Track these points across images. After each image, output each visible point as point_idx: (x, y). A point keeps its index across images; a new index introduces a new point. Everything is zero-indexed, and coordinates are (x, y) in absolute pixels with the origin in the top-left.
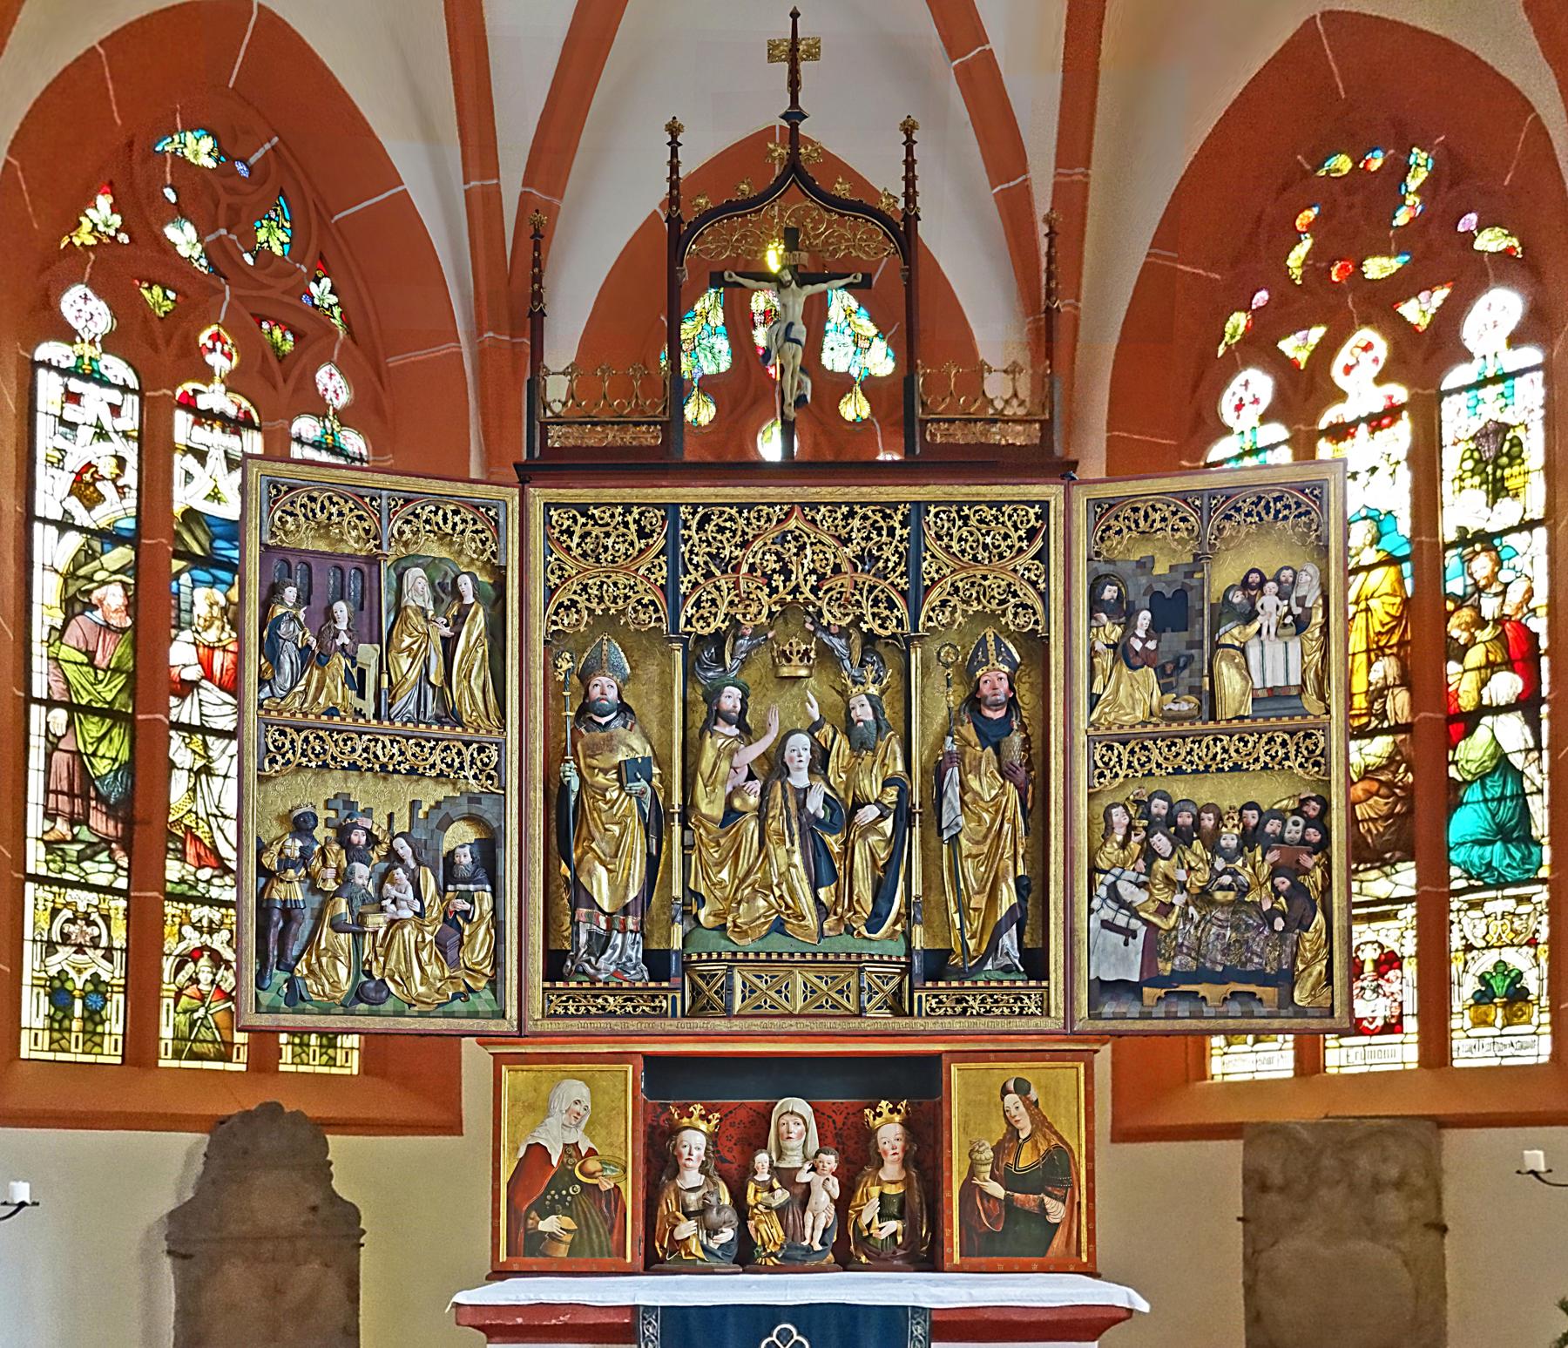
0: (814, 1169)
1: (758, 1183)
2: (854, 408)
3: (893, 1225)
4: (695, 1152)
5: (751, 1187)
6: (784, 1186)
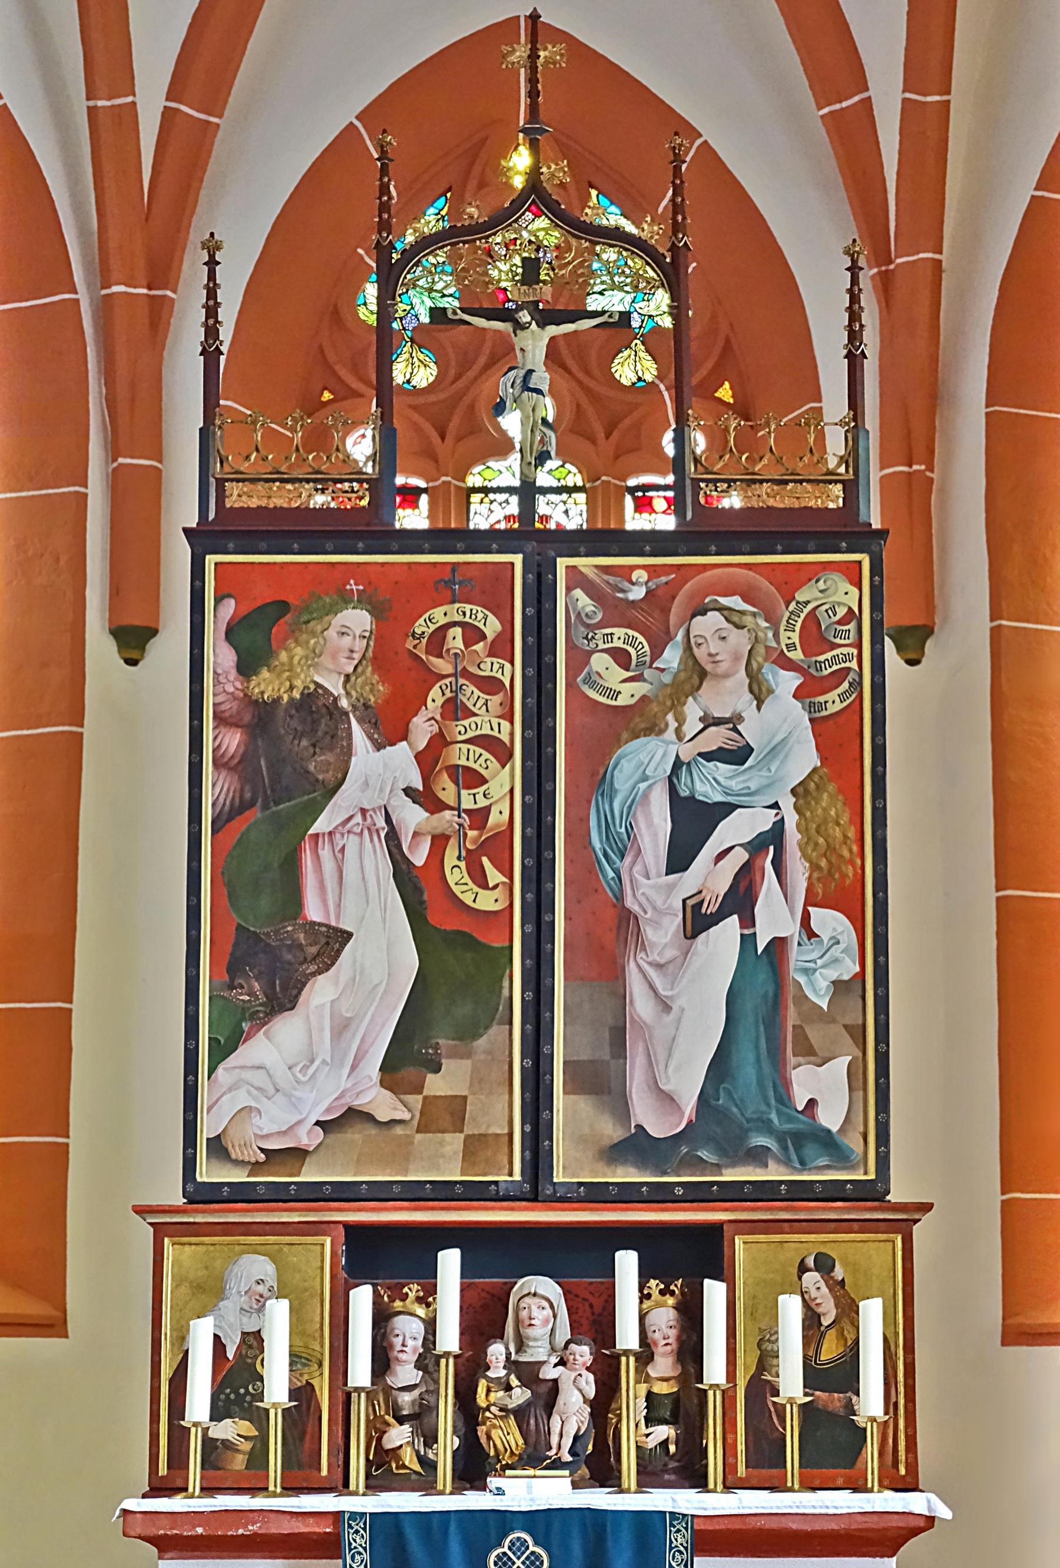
0: (562, 1362)
1: (490, 1380)
2: (633, 367)
3: (663, 1432)
4: (410, 1343)
5: (482, 1385)
6: (524, 1384)
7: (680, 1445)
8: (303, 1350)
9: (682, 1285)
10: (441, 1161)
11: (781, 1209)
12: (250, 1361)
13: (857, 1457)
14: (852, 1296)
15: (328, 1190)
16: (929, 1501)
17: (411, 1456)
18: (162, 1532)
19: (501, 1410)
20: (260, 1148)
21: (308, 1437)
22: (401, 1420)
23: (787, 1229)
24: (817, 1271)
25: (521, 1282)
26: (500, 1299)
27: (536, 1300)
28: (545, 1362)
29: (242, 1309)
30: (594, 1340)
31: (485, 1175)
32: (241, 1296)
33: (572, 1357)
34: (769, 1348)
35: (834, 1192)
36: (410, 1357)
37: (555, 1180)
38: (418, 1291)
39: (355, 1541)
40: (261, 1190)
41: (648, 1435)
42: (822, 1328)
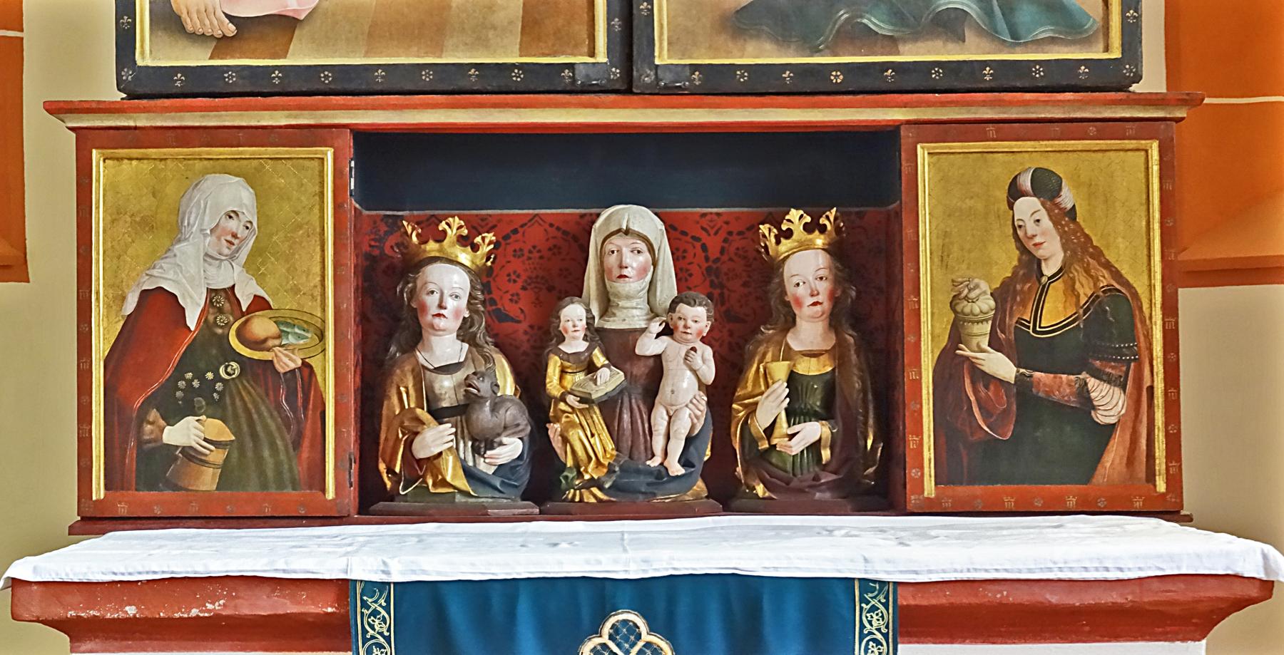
0: (668, 331)
1: (566, 357)
3: (814, 431)
4: (450, 303)
6: (614, 362)
7: (837, 450)
8: (296, 315)
9: (836, 219)
10: (491, 34)
11: (984, 104)
12: (220, 331)
13: (1095, 469)
14: (1087, 231)
15: (327, 79)
16: (1265, 557)
17: (454, 468)
18: (72, 613)
19: (582, 401)
20: (227, 16)
21: (306, 443)
22: (439, 415)
23: (992, 134)
24: (1035, 195)
25: (606, 214)
26: (575, 238)
27: (629, 240)
28: (643, 330)
29: (206, 255)
30: (710, 296)
31: (554, 54)
32: (205, 236)
33: (681, 323)
34: (967, 310)
35: (1060, 79)
36: (450, 323)
37: (657, 62)
38: (460, 227)
39: (372, 627)
40: (231, 78)
41: (792, 436)
42: (1044, 280)
